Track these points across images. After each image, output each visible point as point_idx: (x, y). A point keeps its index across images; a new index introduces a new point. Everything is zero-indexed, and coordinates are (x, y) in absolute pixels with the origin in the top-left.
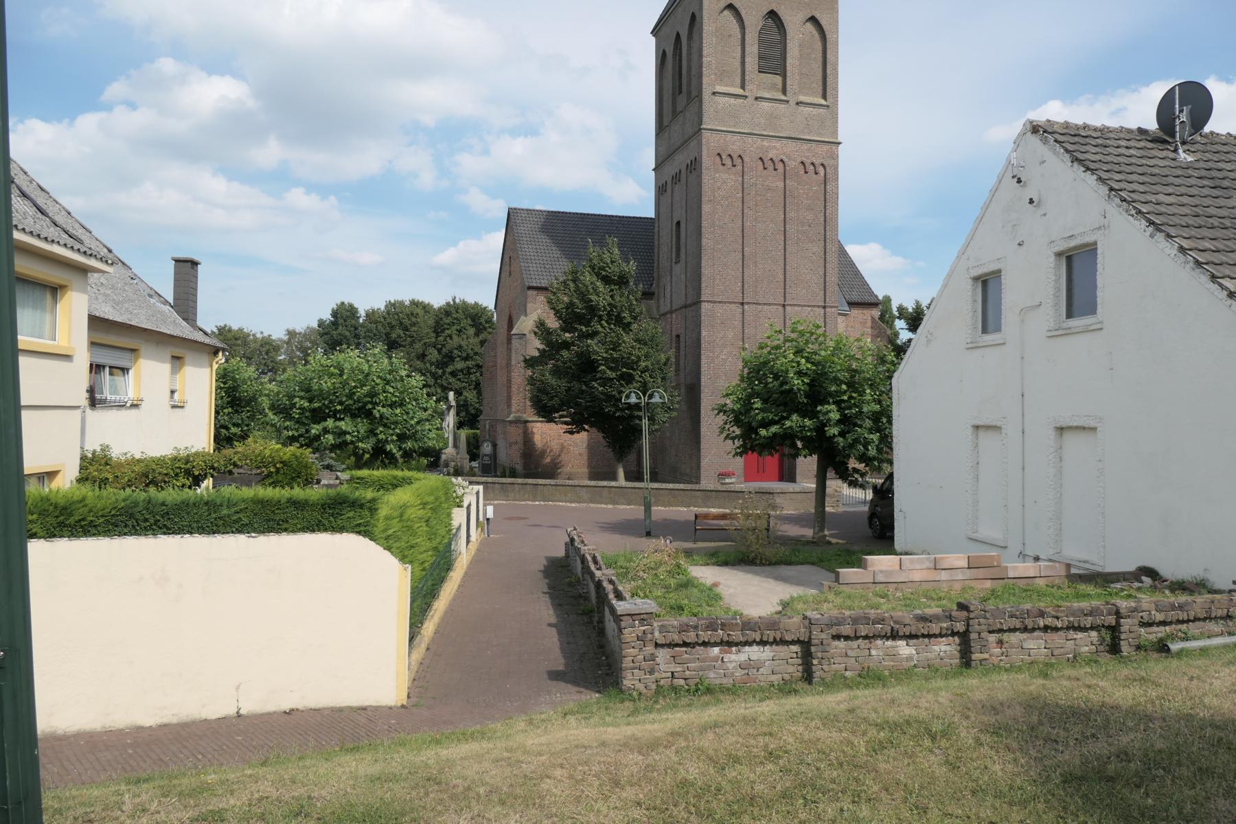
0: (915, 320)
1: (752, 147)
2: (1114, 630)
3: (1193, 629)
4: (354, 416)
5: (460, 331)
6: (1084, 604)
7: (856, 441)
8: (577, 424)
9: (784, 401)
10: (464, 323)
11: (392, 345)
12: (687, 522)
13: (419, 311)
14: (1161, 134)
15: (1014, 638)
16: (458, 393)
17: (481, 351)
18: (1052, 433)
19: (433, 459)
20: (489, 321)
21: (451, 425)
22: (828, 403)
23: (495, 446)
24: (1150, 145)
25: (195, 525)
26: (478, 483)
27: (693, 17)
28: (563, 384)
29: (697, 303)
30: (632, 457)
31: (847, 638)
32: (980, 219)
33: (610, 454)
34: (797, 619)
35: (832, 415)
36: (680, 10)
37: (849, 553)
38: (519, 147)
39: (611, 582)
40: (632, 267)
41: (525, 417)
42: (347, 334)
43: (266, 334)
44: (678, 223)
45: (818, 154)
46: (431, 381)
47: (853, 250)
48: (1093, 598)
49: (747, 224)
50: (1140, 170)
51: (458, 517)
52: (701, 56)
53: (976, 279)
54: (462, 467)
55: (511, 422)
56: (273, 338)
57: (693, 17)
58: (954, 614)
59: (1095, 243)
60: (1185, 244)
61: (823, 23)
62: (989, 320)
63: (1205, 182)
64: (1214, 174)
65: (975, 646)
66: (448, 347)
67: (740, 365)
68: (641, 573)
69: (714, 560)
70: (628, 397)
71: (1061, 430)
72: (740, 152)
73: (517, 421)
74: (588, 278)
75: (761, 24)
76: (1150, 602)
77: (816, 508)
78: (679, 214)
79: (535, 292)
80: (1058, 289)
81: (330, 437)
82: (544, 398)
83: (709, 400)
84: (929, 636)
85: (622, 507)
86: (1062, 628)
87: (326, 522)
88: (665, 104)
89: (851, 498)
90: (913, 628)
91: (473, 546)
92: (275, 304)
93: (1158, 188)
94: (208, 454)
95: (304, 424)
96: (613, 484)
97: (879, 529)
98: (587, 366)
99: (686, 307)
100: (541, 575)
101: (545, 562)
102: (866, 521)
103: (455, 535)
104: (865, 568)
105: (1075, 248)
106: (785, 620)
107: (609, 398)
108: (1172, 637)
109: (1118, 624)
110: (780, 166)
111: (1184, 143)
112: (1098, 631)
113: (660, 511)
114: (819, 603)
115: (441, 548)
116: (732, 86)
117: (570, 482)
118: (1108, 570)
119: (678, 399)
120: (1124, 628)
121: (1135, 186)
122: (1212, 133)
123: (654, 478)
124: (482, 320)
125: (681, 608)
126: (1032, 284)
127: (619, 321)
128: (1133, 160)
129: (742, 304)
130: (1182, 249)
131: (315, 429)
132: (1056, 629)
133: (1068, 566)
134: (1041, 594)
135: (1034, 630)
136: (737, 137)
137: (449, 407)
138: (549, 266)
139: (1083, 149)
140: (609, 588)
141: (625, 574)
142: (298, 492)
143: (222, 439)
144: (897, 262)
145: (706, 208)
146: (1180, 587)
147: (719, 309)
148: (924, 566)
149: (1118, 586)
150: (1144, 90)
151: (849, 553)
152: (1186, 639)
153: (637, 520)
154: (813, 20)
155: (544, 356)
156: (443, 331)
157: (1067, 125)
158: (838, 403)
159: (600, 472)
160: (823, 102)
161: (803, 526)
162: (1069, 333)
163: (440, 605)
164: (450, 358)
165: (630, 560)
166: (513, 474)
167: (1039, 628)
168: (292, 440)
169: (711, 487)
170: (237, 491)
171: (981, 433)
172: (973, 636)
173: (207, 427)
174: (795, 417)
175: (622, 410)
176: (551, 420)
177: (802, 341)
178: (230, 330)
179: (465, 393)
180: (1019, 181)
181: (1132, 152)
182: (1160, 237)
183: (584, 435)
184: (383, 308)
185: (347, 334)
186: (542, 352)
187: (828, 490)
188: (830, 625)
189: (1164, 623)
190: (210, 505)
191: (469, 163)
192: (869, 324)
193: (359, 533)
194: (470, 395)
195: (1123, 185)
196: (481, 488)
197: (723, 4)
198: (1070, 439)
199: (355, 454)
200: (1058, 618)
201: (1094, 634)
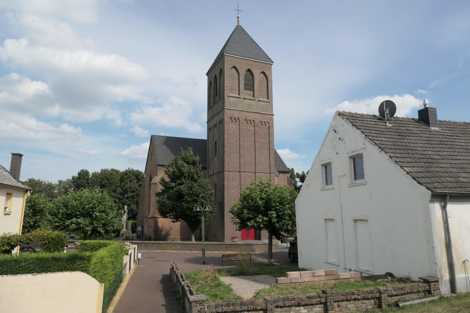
0: (303, 178)
1: (243, 116)
2: (379, 299)
3: (407, 297)
4: (84, 217)
5: (131, 181)
6: (368, 289)
7: (283, 225)
8: (176, 218)
9: (256, 210)
10: (132, 178)
11: (102, 186)
12: (220, 257)
13: (114, 173)
14: (380, 117)
15: (344, 304)
16: (129, 206)
17: (139, 189)
18: (352, 222)
19: (117, 234)
20: (143, 177)
21: (125, 219)
22: (273, 211)
23: (143, 227)
24: (377, 121)
25: (9, 270)
26: (135, 244)
27: (221, 70)
28: (171, 202)
29: (223, 171)
30: (198, 231)
31: (281, 307)
32: (323, 144)
33: (189, 230)
34: (261, 300)
35: (273, 215)
36: (216, 67)
37: (282, 269)
38: (154, 111)
39: (188, 286)
40: (197, 158)
41: (156, 216)
42: (84, 182)
43: (49, 182)
44: (216, 142)
45: (266, 118)
46: (117, 201)
47: (279, 152)
48: (371, 287)
49: (241, 143)
50: (375, 129)
51: (126, 259)
52: (224, 83)
53: (323, 165)
54: (129, 236)
55: (150, 218)
56: (53, 183)
57: (221, 70)
58: (321, 295)
59: (362, 154)
60: (392, 155)
61: (267, 74)
62: (328, 180)
63: (396, 134)
64: (399, 131)
65: (329, 308)
66: (126, 187)
67: (239, 195)
68: (200, 281)
69: (230, 274)
70: (196, 208)
71: (355, 221)
72: (238, 117)
73: (152, 218)
74: (180, 162)
75: (245, 73)
76: (391, 287)
77: (269, 251)
78: (216, 139)
79: (161, 167)
80: (351, 170)
81: (74, 225)
82: (163, 209)
83: (227, 209)
84: (312, 305)
85: (194, 252)
86: (360, 299)
87: (68, 267)
88: (211, 100)
89: (281, 246)
90: (306, 301)
91: (132, 271)
92: (54, 170)
93: (381, 135)
94: (19, 236)
95: (63, 220)
96: (190, 242)
97: (292, 260)
98: (180, 196)
99: (219, 173)
100: (160, 283)
101: (162, 277)
102: (288, 256)
103: (124, 267)
104: (287, 277)
105: (356, 155)
106: (257, 301)
107: (189, 208)
108: (399, 300)
109: (381, 297)
110: (253, 122)
111: (388, 120)
112: (374, 299)
113: (209, 253)
114: (270, 292)
115: (118, 273)
116: (235, 94)
117: (173, 242)
118: (376, 274)
119: (215, 208)
120: (383, 298)
121: (374, 135)
122: (397, 117)
123: (207, 239)
124: (140, 177)
125: (216, 296)
126: (341, 168)
127: (193, 179)
128: (372, 126)
129: (240, 172)
130: (390, 157)
131: (68, 222)
132: (359, 300)
133: (361, 273)
134: (353, 285)
135: (350, 300)
136: (237, 112)
137: (125, 212)
138: (166, 157)
139: (356, 121)
140: (187, 289)
141: (194, 281)
142: (56, 254)
143: (27, 227)
144: (295, 156)
145: (226, 137)
146: (401, 280)
147: (231, 174)
148: (309, 275)
149: (379, 280)
150: (376, 98)
151: (282, 269)
152: (405, 301)
153: (200, 257)
154: (263, 73)
155: (163, 192)
156: (123, 181)
157: (350, 113)
158: (276, 210)
159: (185, 237)
160: (267, 101)
161: (264, 258)
162: (356, 185)
163: (116, 299)
164: (126, 191)
165: (196, 275)
166: (150, 239)
167: (352, 300)
168: (56, 228)
169: (229, 243)
170: (29, 255)
171: (328, 222)
172: (329, 304)
173: (20, 222)
174: (260, 216)
175: (194, 213)
176: (167, 217)
177: (263, 187)
178: (34, 180)
179: (132, 206)
180: (335, 132)
181: (372, 123)
182: (383, 152)
183: (179, 223)
184: (100, 172)
185: (84, 182)
186: (163, 190)
187: (273, 243)
188: (274, 302)
189: (396, 295)
190: (17, 261)
191: (136, 116)
192: (286, 179)
193: (82, 271)
194: (134, 206)
195: (370, 134)
196: (136, 246)
197: (232, 66)
198: (359, 224)
199: (84, 232)
200: (359, 295)
201: (372, 301)
